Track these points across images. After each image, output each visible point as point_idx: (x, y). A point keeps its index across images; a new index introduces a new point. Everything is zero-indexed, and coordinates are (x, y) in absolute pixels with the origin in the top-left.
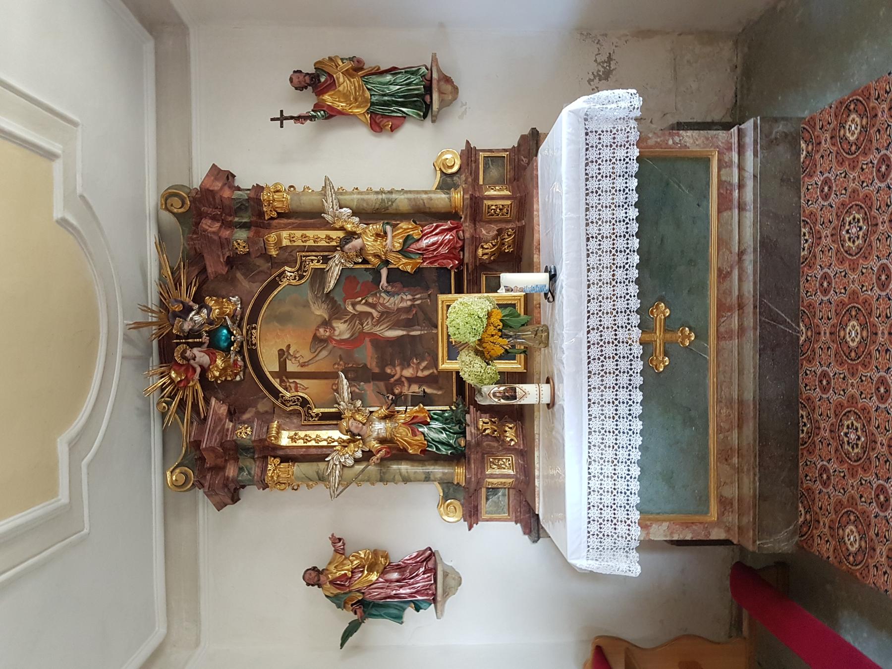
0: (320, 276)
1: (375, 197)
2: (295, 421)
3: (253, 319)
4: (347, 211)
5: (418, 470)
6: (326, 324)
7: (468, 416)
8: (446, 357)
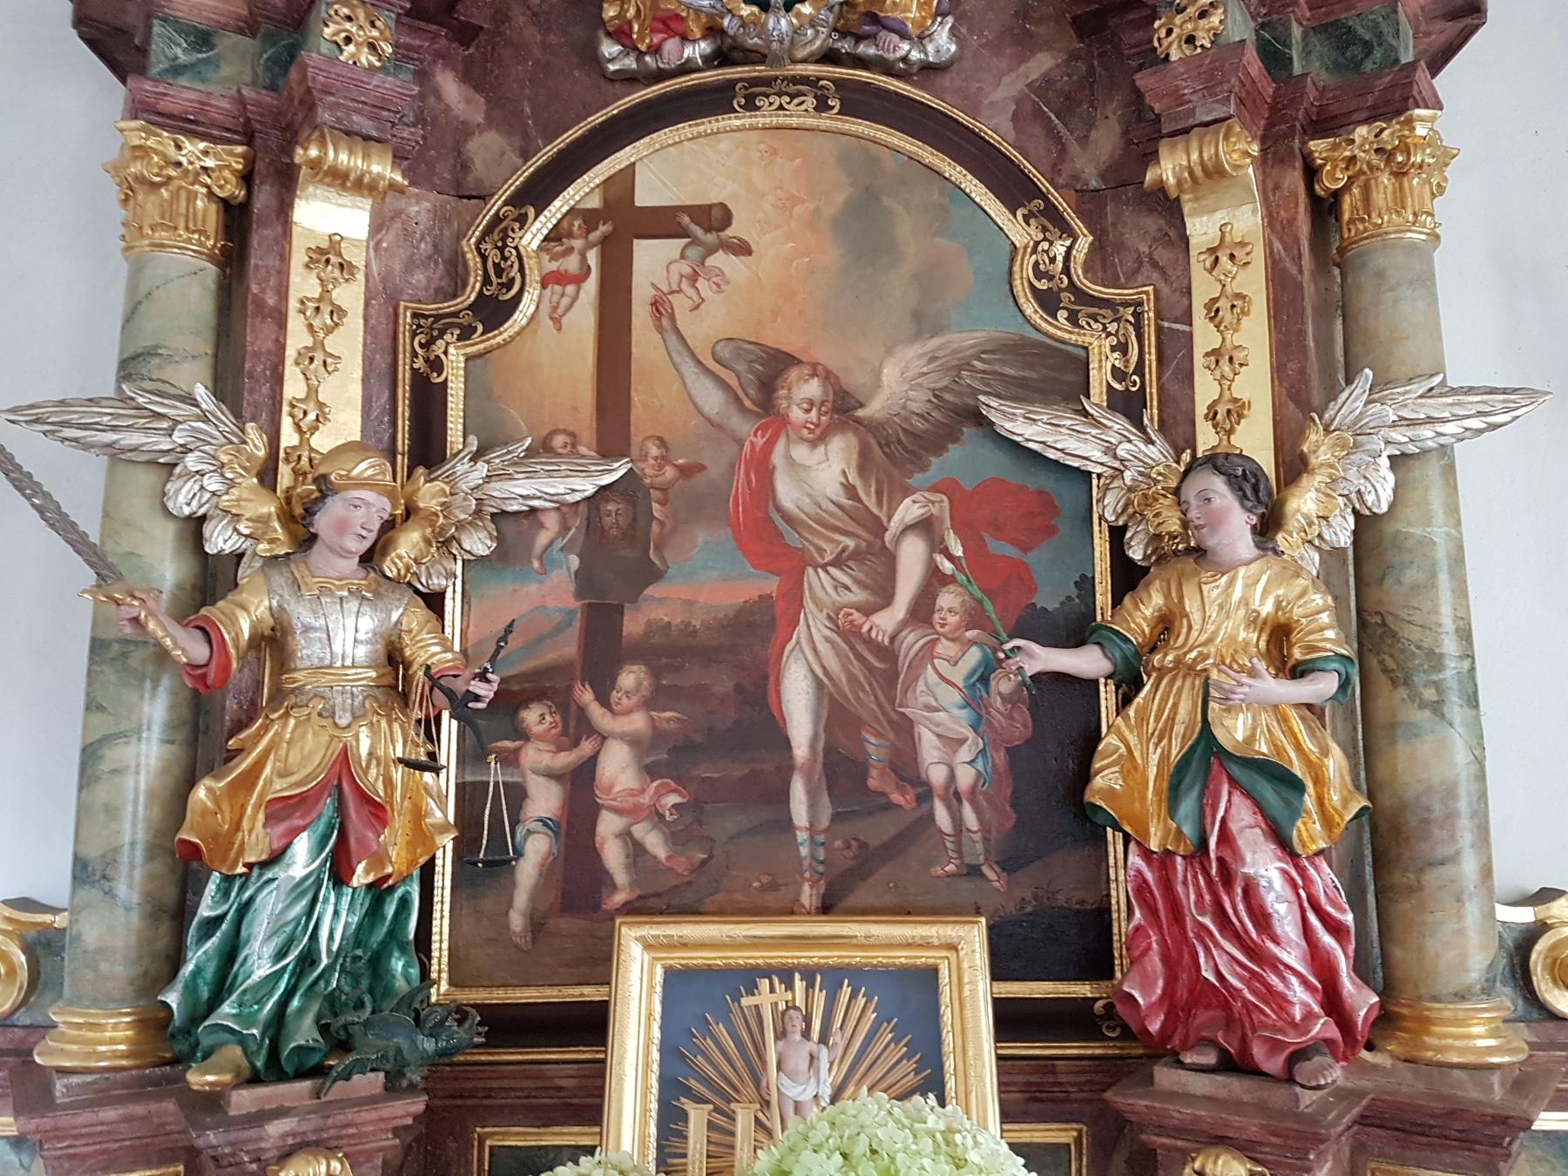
0: (1062, 380)
1: (1448, 624)
2: (419, 278)
3: (860, 102)
4: (1381, 492)
5: (133, 827)
6: (842, 408)
7: (371, 1082)
8: (678, 958)
